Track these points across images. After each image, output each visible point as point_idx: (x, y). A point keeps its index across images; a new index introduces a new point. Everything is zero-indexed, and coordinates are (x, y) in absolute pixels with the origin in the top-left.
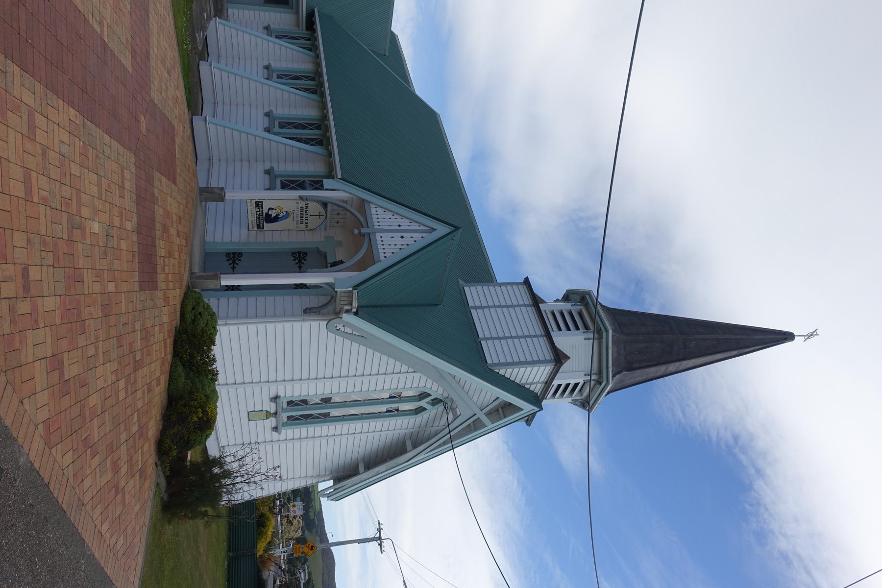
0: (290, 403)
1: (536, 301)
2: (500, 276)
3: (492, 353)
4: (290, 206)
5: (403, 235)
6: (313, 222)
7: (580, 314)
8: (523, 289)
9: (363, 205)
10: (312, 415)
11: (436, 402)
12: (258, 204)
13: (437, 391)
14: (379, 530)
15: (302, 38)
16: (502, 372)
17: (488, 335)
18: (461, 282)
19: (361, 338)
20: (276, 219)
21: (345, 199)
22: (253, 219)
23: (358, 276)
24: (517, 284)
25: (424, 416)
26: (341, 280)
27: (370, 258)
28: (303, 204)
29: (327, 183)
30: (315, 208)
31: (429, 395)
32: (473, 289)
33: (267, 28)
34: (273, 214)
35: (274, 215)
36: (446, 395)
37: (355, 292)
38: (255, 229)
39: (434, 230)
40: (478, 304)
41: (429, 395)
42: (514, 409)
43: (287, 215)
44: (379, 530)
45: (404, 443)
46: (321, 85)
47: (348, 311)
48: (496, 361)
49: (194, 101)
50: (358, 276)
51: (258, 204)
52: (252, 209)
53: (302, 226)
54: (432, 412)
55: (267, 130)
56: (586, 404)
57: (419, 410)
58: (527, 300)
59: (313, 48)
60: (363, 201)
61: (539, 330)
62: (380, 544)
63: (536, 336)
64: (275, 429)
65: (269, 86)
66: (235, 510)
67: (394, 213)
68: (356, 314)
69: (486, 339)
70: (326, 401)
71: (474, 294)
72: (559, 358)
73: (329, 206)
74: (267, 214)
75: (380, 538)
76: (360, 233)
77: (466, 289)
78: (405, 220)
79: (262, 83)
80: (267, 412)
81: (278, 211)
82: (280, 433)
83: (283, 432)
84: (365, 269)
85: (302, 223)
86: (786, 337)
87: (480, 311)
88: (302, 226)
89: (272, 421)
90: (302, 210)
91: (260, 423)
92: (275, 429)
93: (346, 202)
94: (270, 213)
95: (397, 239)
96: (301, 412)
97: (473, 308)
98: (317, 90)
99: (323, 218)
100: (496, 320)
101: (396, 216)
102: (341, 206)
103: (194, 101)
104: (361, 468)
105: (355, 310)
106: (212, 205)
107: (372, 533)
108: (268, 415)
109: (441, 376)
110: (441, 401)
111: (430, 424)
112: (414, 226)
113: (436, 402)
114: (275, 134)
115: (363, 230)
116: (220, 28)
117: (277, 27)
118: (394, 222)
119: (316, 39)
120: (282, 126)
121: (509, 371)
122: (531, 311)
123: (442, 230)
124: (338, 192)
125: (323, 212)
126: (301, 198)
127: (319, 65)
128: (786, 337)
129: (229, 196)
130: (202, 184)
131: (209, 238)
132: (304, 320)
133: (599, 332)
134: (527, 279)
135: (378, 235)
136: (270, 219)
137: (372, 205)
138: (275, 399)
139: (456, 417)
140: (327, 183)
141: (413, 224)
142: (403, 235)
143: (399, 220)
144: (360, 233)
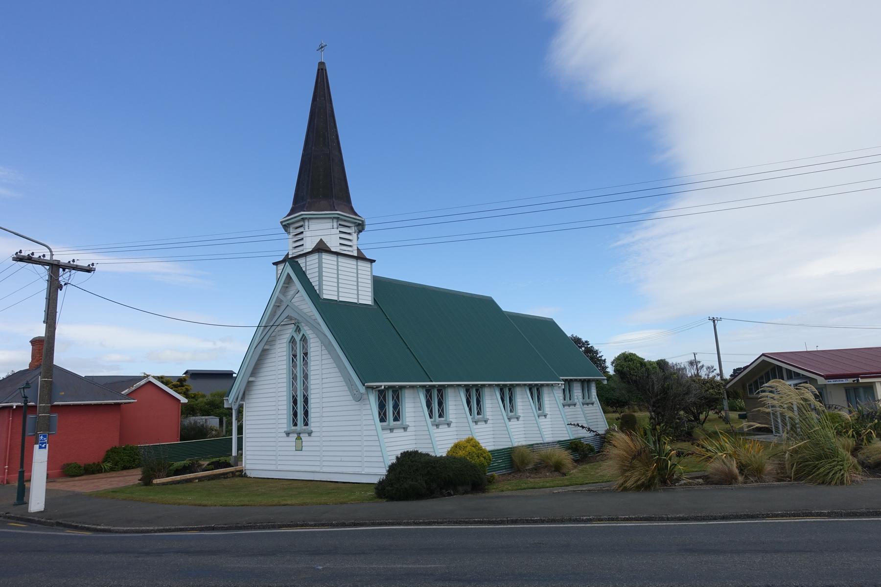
64: (310, 434)
86: (322, 72)
89: (304, 437)
92: (310, 434)
108: (299, 438)
128: (322, 72)
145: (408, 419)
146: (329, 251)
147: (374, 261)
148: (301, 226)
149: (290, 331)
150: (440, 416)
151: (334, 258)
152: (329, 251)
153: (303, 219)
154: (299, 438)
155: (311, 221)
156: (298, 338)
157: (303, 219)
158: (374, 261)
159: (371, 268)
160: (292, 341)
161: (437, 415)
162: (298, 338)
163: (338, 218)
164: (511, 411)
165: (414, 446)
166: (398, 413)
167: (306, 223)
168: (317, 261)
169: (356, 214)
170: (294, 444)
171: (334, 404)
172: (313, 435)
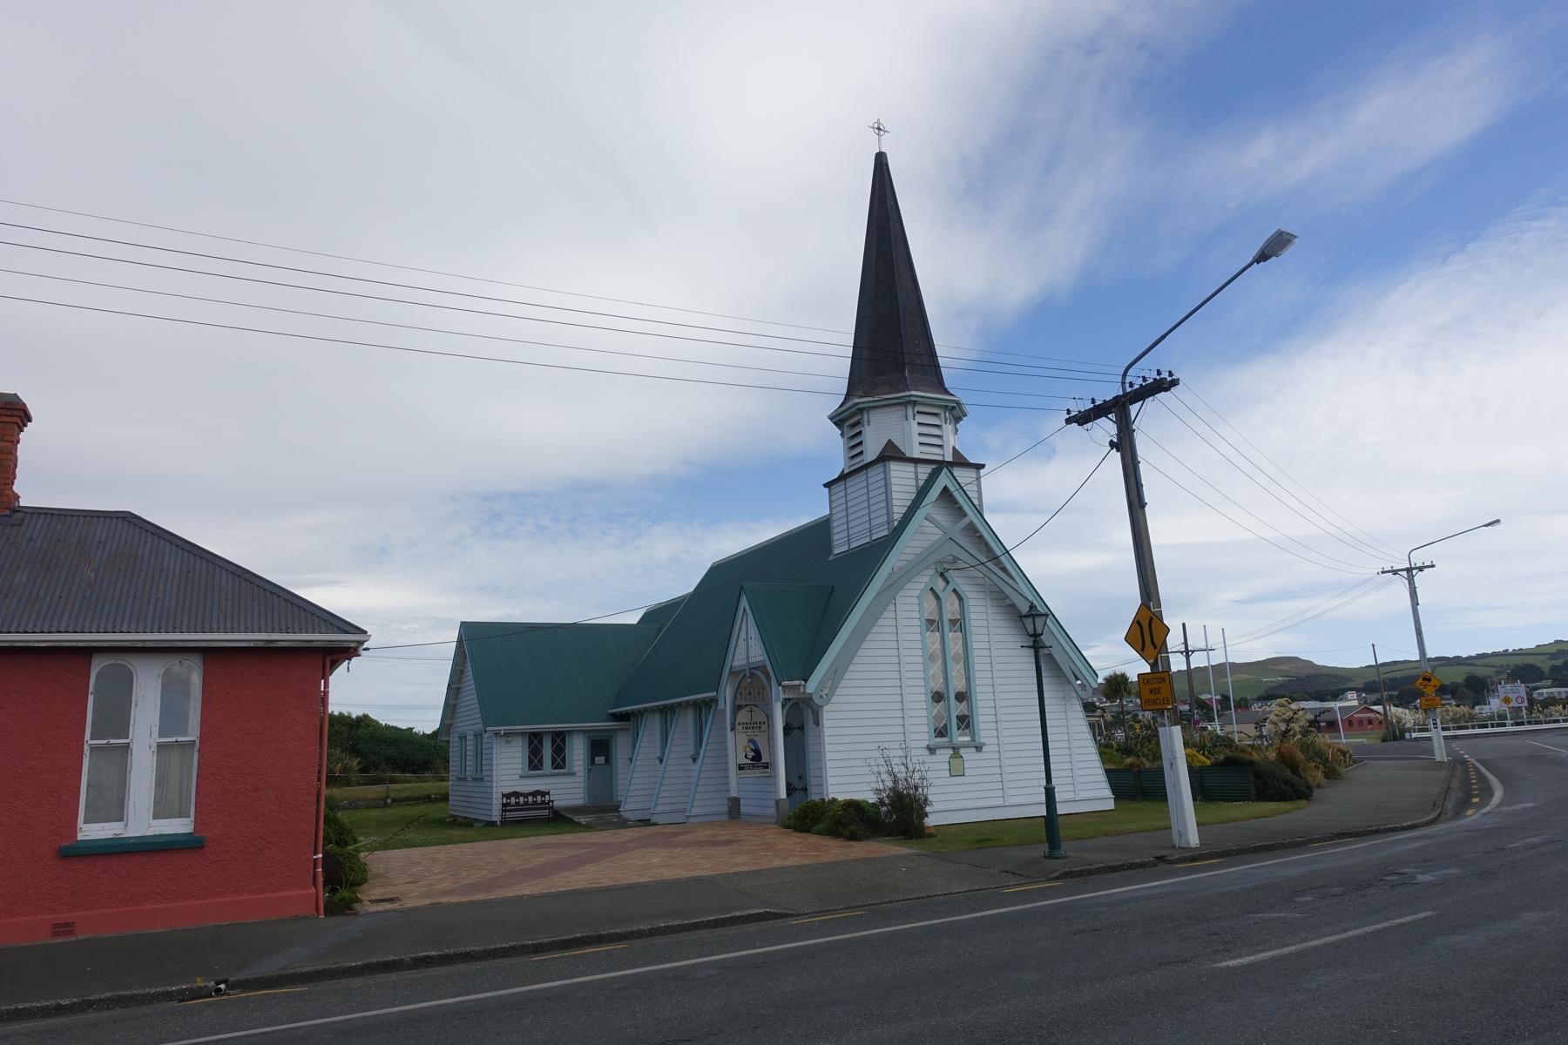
1: (843, 477)
2: (824, 511)
3: (883, 532)
4: (743, 740)
6: (759, 716)
8: (836, 489)
9: (732, 673)
12: (741, 767)
14: (1395, 572)
19: (837, 674)
22: (757, 772)
27: (763, 669)
28: (739, 728)
42: (946, 489)
43: (752, 741)
44: (1395, 572)
49: (646, 823)
51: (741, 767)
52: (747, 773)
53: (764, 727)
59: (641, 713)
61: (861, 477)
62: (1421, 569)
64: (979, 748)
66: (1119, 792)
70: (938, 697)
72: (891, 453)
75: (1409, 570)
86: (881, 162)
88: (764, 727)
92: (979, 748)
96: (955, 719)
102: (737, 692)
103: (646, 823)
106: (743, 809)
107: (1401, 585)
108: (956, 754)
116: (628, 807)
124: (727, 694)
127: (687, 703)
128: (881, 162)
129: (734, 794)
130: (726, 817)
133: (861, 411)
134: (825, 485)
136: (757, 756)
138: (932, 750)
139: (956, 560)
145: (982, 734)
147: (983, 466)
151: (910, 467)
153: (861, 411)
154: (956, 754)
158: (983, 466)
159: (978, 479)
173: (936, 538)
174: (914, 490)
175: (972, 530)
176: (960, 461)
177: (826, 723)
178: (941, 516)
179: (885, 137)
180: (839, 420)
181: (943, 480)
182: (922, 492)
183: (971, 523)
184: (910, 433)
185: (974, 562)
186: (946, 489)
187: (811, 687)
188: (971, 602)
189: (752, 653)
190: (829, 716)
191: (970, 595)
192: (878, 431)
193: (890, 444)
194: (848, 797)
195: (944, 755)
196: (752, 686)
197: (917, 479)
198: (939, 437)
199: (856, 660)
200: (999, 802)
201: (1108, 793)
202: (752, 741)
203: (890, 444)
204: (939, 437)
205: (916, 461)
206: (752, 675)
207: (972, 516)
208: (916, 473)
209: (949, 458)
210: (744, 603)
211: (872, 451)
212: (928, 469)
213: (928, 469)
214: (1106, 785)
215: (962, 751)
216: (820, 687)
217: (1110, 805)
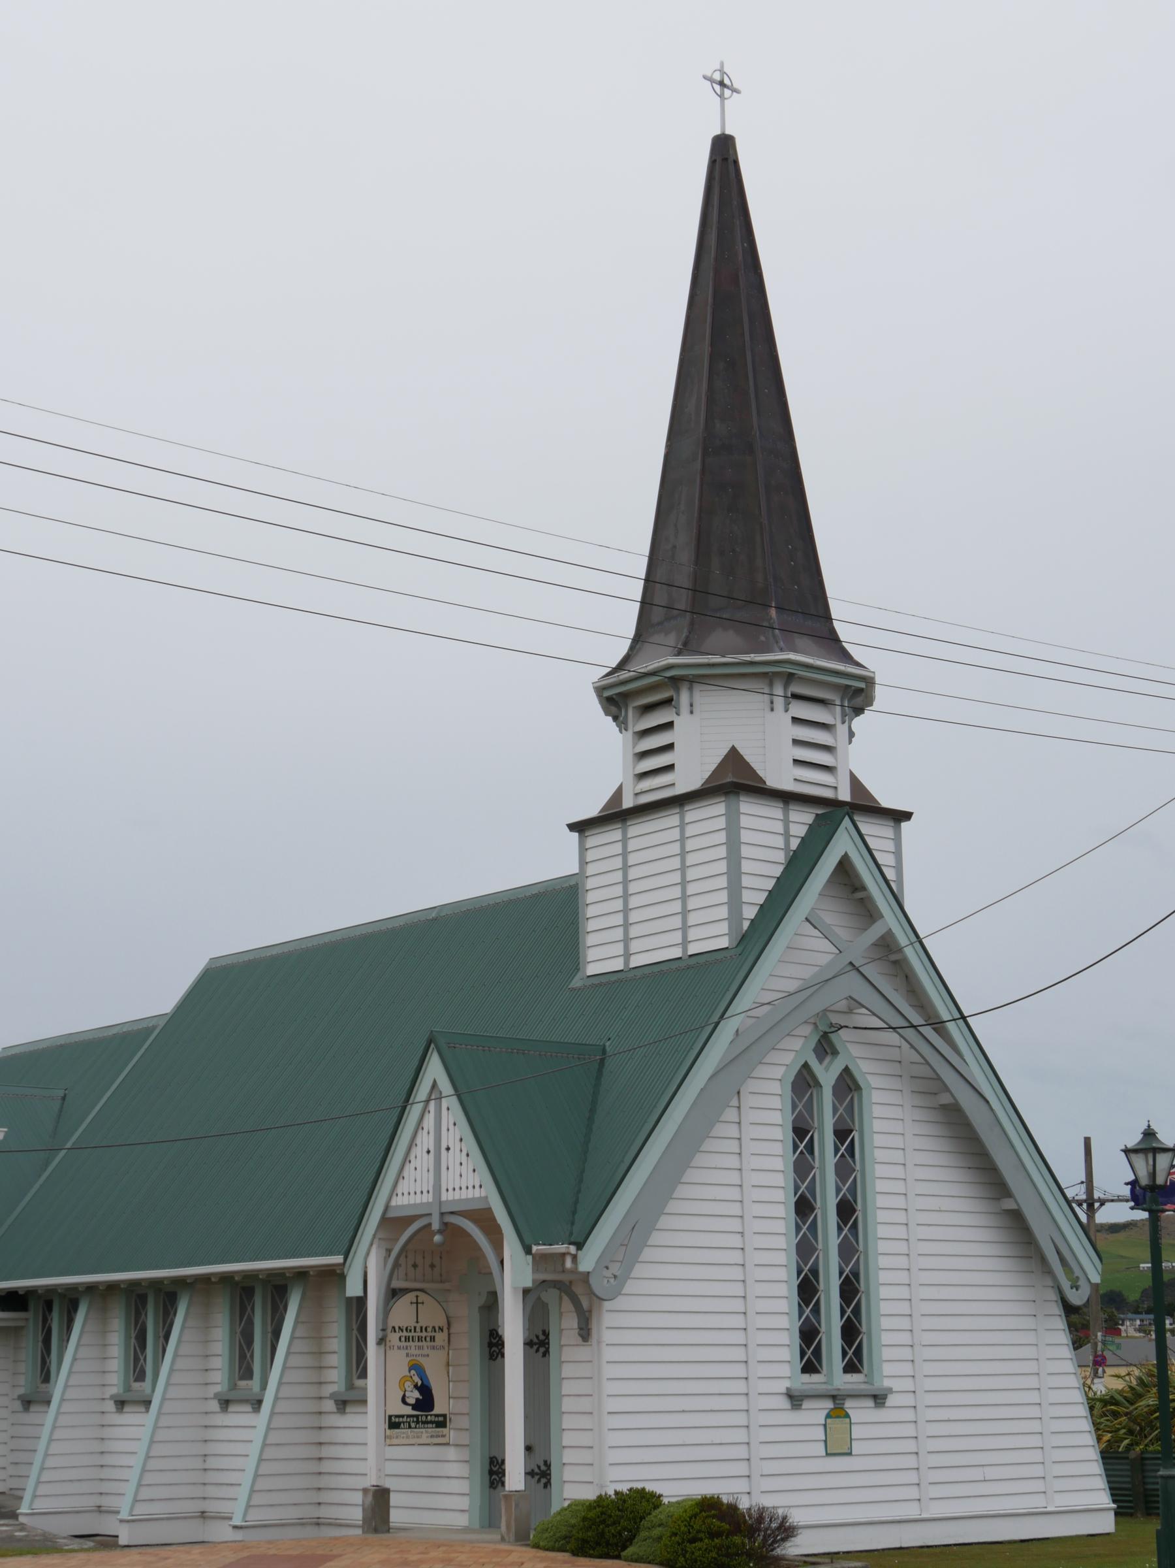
0: (810, 1367)
1: (615, 815)
3: (712, 935)
4: (399, 1364)
5: (444, 1146)
7: (649, 708)
8: (595, 839)
9: (392, 1223)
10: (363, 1374)
11: (825, 1047)
13: (793, 1051)
15: (45, 1320)
16: (750, 913)
17: (677, 937)
18: (576, 983)
20: (425, 1391)
21: (383, 1253)
22: (425, 1434)
23: (511, 1245)
24: (583, 850)
25: (868, 1071)
26: (515, 1272)
28: (393, 1338)
29: (353, 1288)
30: (403, 1314)
31: (806, 1066)
32: (591, 955)
33: (27, 1403)
34: (414, 1396)
35: (417, 1394)
36: (807, 1030)
37: (535, 1248)
38: (445, 1431)
39: (434, 1085)
40: (619, 949)
41: (806, 1066)
42: (844, 867)
43: (416, 1367)
45: (944, 1107)
46: (156, 1284)
47: (574, 1258)
48: (724, 928)
50: (511, 1245)
51: (394, 1424)
53: (441, 1338)
54: (854, 1052)
55: (257, 1404)
56: (857, 694)
57: (848, 1085)
58: (613, 834)
60: (385, 1221)
61: (669, 820)
63: (682, 826)
64: (879, 1399)
65: (164, 1399)
67: (406, 1159)
68: (580, 1246)
69: (685, 943)
71: (601, 956)
72: (735, 781)
73: (396, 1284)
74: (414, 1407)
76: (440, 1232)
77: (592, 970)
78: (418, 1140)
79: (159, 1413)
80: (828, 1416)
81: (409, 1386)
82: (890, 1390)
83: (887, 1383)
84: (498, 1226)
85: (433, 1339)
86: (723, 154)
87: (635, 946)
88: (441, 1338)
89: (859, 1411)
90: (407, 1339)
91: (857, 1432)
92: (879, 1399)
93: (389, 1251)
94: (412, 1401)
95: (451, 1159)
97: (627, 962)
98: (167, 1295)
99: (423, 1297)
100: (659, 906)
101: (412, 1157)
104: (1009, 1204)
105: (573, 1249)
106: (396, 1517)
108: (838, 1412)
109: (743, 1059)
110: (825, 1035)
111: (895, 1054)
112: (429, 1121)
113: (825, 1047)
114: (264, 1386)
115: (436, 1226)
117: (22, 1380)
118: (421, 1161)
119: (51, 1290)
120: (248, 1374)
121: (747, 896)
122: (636, 828)
123: (434, 1070)
124: (368, 1269)
125: (411, 1297)
126: (381, 1341)
128: (723, 154)
131: (462, 1520)
132: (599, 1342)
134: (573, 827)
135: (444, 1198)
136: (425, 1401)
137: (393, 1203)
138: (795, 1399)
139: (854, 1004)
140: (353, 1288)
141: (425, 1124)
142: (444, 1146)
143: (418, 1151)
144: (440, 1232)
145: (887, 1369)
146: (760, 790)
147: (907, 816)
148: (668, 702)
149: (797, 1044)
150: (851, 1367)
151: (774, 811)
152: (760, 790)
153: (676, 682)
154: (838, 1412)
155: (697, 688)
156: (827, 1075)
157: (676, 682)
158: (907, 816)
159: (898, 840)
160: (804, 1082)
161: (838, 1363)
162: (827, 1075)
163: (790, 678)
164: (851, 1367)
165: (739, 1486)
166: (858, 1353)
167: (684, 698)
168: (721, 823)
169: (846, 657)
170: (819, 1434)
171: (945, 1293)
172: (891, 1400)
173: (824, 960)
174: (781, 857)
175: (887, 947)
176: (863, 805)
177: (608, 1336)
178: (835, 918)
179: (733, 101)
180: (617, 698)
181: (842, 844)
182: (799, 864)
183: (890, 933)
184: (768, 734)
185: (898, 1022)
186: (844, 867)
187: (588, 1260)
188: (876, 1096)
189: (449, 1179)
190: (612, 1322)
191: (874, 1081)
192: (703, 734)
193: (734, 758)
194: (639, 1486)
195: (815, 1413)
196: (441, 1256)
197: (787, 835)
198: (827, 748)
199: (672, 1206)
200: (912, 1511)
201: (1104, 1499)
202: (416, 1367)
203: (734, 758)
204: (827, 748)
205: (787, 798)
206: (446, 1227)
207: (890, 920)
208: (786, 822)
209: (845, 795)
210: (434, 1070)
211: (691, 772)
212: (802, 820)
213: (802, 820)
214: (1101, 1483)
215: (849, 1404)
216: (604, 1263)
217: (1106, 1523)
